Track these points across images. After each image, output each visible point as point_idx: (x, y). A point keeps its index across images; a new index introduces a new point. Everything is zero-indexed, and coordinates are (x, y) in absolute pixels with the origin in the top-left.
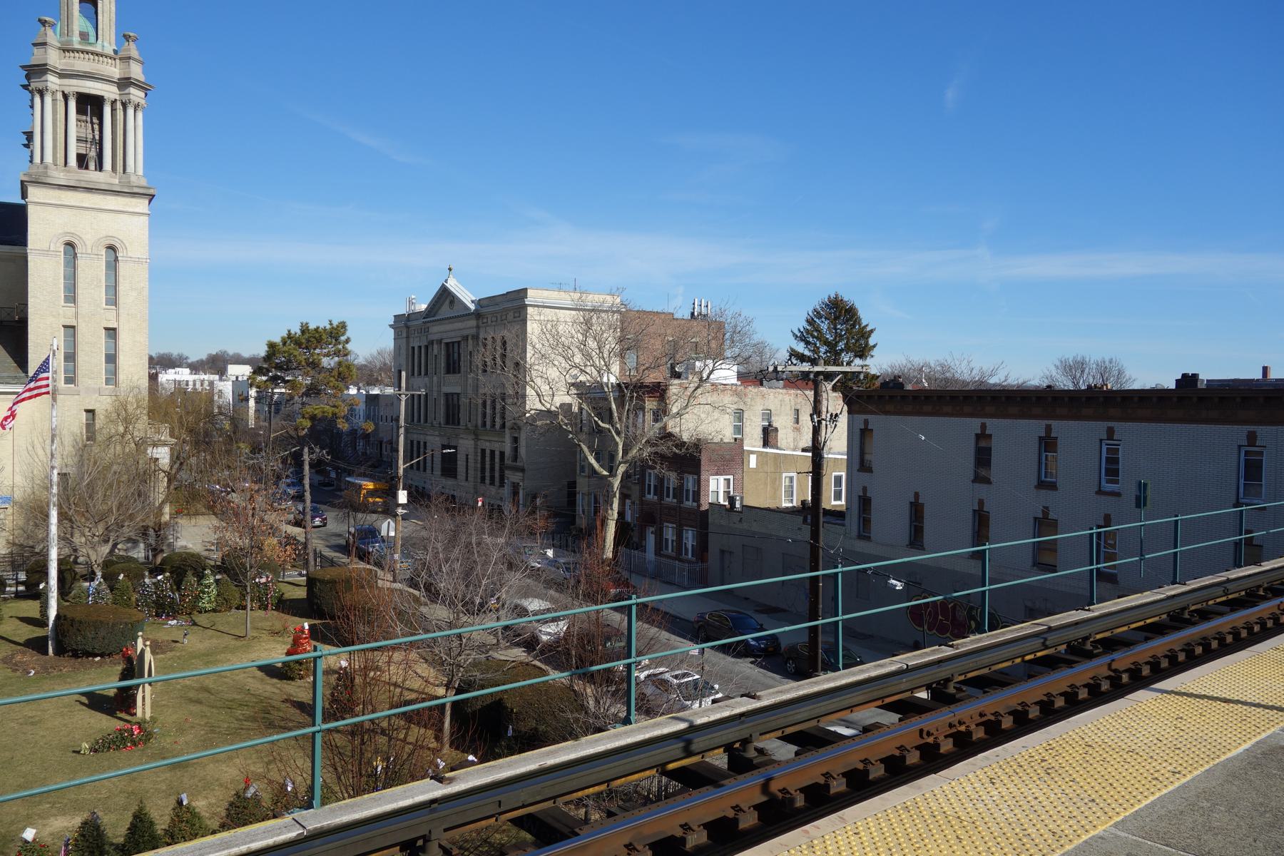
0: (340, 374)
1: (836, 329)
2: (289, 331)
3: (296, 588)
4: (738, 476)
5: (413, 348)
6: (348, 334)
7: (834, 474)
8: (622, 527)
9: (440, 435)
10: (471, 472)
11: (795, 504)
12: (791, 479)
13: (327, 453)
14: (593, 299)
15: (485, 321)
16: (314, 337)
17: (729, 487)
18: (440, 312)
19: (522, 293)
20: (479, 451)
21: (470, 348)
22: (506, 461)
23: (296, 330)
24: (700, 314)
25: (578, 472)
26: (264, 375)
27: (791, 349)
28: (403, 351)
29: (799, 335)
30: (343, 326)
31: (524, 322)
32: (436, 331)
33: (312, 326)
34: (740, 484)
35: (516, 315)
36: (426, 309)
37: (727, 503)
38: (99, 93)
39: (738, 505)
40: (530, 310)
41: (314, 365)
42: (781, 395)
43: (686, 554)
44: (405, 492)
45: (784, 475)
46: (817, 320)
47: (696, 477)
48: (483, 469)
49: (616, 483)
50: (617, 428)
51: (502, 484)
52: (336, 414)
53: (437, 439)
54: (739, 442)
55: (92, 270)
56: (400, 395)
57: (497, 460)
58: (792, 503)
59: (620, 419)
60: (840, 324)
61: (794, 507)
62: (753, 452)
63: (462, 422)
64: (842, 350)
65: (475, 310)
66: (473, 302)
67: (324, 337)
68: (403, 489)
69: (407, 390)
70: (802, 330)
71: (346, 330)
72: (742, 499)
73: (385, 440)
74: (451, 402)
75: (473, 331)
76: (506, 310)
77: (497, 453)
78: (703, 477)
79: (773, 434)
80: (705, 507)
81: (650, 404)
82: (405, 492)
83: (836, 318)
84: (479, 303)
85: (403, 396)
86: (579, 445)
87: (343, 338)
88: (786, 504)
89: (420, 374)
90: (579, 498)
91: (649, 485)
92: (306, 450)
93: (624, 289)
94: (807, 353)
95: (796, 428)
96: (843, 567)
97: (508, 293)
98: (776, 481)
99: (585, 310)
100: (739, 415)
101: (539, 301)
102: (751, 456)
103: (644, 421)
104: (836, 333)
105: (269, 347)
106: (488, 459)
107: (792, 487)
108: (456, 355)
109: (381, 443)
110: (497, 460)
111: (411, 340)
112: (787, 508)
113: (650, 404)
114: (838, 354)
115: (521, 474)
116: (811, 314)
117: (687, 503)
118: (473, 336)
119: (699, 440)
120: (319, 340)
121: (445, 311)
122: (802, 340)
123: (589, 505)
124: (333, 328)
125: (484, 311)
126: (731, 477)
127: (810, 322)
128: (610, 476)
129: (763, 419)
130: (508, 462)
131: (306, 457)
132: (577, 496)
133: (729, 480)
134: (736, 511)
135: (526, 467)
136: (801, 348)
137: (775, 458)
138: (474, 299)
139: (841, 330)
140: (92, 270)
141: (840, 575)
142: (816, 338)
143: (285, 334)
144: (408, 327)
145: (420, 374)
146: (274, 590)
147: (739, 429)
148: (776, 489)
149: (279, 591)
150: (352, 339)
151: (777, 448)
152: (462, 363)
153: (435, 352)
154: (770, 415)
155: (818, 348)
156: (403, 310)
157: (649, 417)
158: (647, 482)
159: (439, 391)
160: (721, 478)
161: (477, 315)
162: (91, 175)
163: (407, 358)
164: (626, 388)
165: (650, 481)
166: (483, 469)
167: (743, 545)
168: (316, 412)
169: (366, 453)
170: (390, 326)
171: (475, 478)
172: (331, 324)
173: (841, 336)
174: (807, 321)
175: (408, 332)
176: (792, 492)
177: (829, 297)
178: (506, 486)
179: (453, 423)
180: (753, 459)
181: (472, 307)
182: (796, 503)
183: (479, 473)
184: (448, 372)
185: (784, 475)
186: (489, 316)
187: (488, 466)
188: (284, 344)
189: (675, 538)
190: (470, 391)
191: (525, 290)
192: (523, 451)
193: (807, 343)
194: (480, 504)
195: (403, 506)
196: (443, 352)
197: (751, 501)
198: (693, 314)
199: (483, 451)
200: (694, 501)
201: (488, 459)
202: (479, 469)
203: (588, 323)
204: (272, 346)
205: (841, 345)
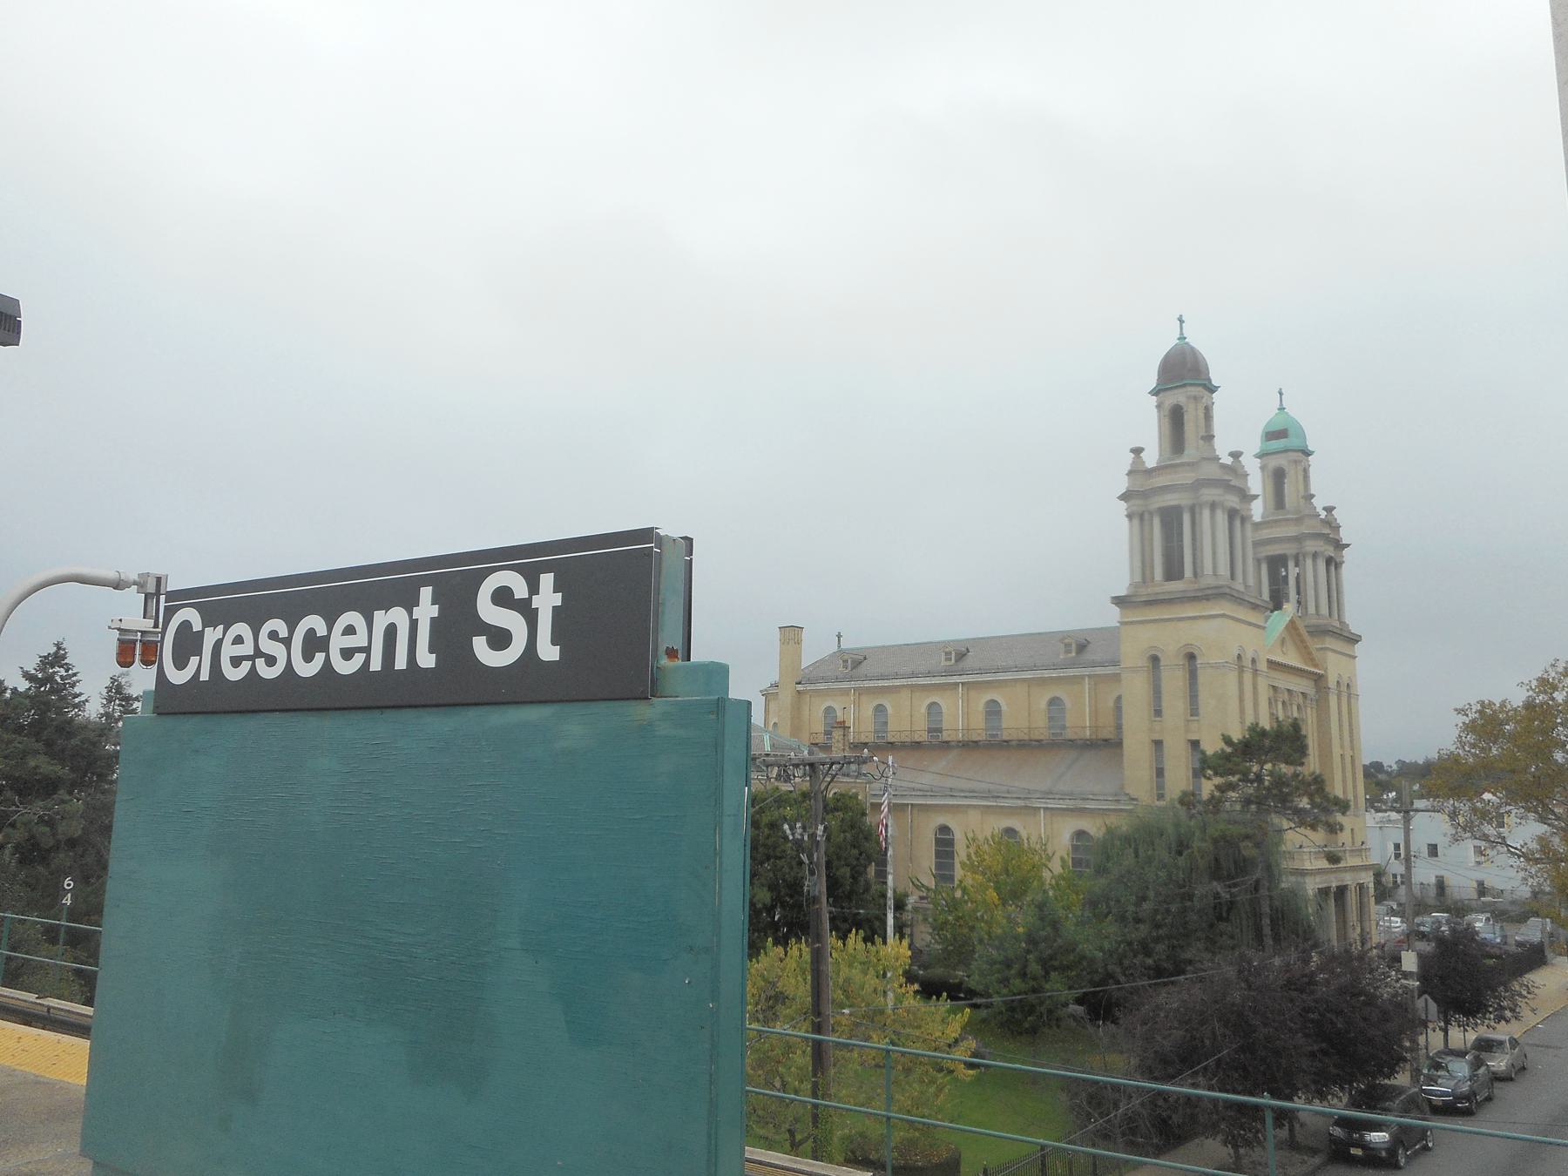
55: (1173, 681)
140: (1173, 681)
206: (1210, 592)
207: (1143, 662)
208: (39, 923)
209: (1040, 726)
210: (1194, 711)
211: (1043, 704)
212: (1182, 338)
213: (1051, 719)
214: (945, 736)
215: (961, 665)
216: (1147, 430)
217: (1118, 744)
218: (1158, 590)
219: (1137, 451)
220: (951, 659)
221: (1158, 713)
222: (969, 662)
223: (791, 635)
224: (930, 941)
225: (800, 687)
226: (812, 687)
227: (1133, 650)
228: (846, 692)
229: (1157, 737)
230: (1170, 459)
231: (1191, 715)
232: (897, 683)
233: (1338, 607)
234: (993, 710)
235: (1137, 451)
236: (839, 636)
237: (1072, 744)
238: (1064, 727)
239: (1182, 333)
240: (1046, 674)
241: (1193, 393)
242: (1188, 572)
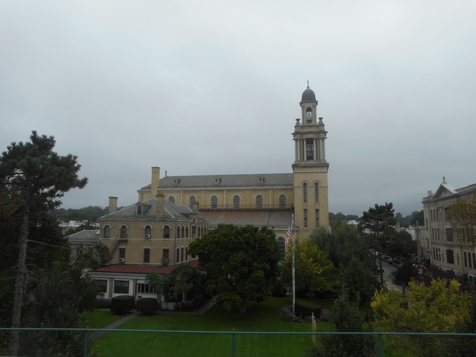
2: (370, 208)
5: (431, 210)
10: (460, 262)
33: (379, 205)
38: (312, 137)
55: (311, 192)
57: (472, 257)
87: (391, 210)
89: (435, 221)
110: (472, 257)
121: (444, 195)
140: (311, 192)
145: (435, 221)
153: (440, 211)
159: (443, 227)
162: (311, 162)
202: (464, 261)
204: (365, 213)
206: (323, 165)
207: (302, 185)
208: (19, 330)
209: (209, 205)
210: (317, 200)
211: (255, 197)
212: (308, 87)
213: (257, 202)
214: (218, 207)
215: (179, 185)
216: (298, 113)
217: (292, 210)
218: (306, 163)
219: (298, 120)
220: (218, 182)
221: (305, 201)
222: (181, 183)
223: (156, 170)
224: (324, 278)
225: (160, 189)
226: (165, 189)
227: (298, 181)
228: (179, 191)
229: (305, 208)
230: (307, 124)
231: (316, 202)
232: (200, 189)
233: (317, 172)
234: (214, 199)
235: (298, 120)
236: (166, 172)
237: (265, 210)
238: (262, 205)
239: (308, 86)
240: (257, 188)
241: (314, 105)
242: (315, 158)
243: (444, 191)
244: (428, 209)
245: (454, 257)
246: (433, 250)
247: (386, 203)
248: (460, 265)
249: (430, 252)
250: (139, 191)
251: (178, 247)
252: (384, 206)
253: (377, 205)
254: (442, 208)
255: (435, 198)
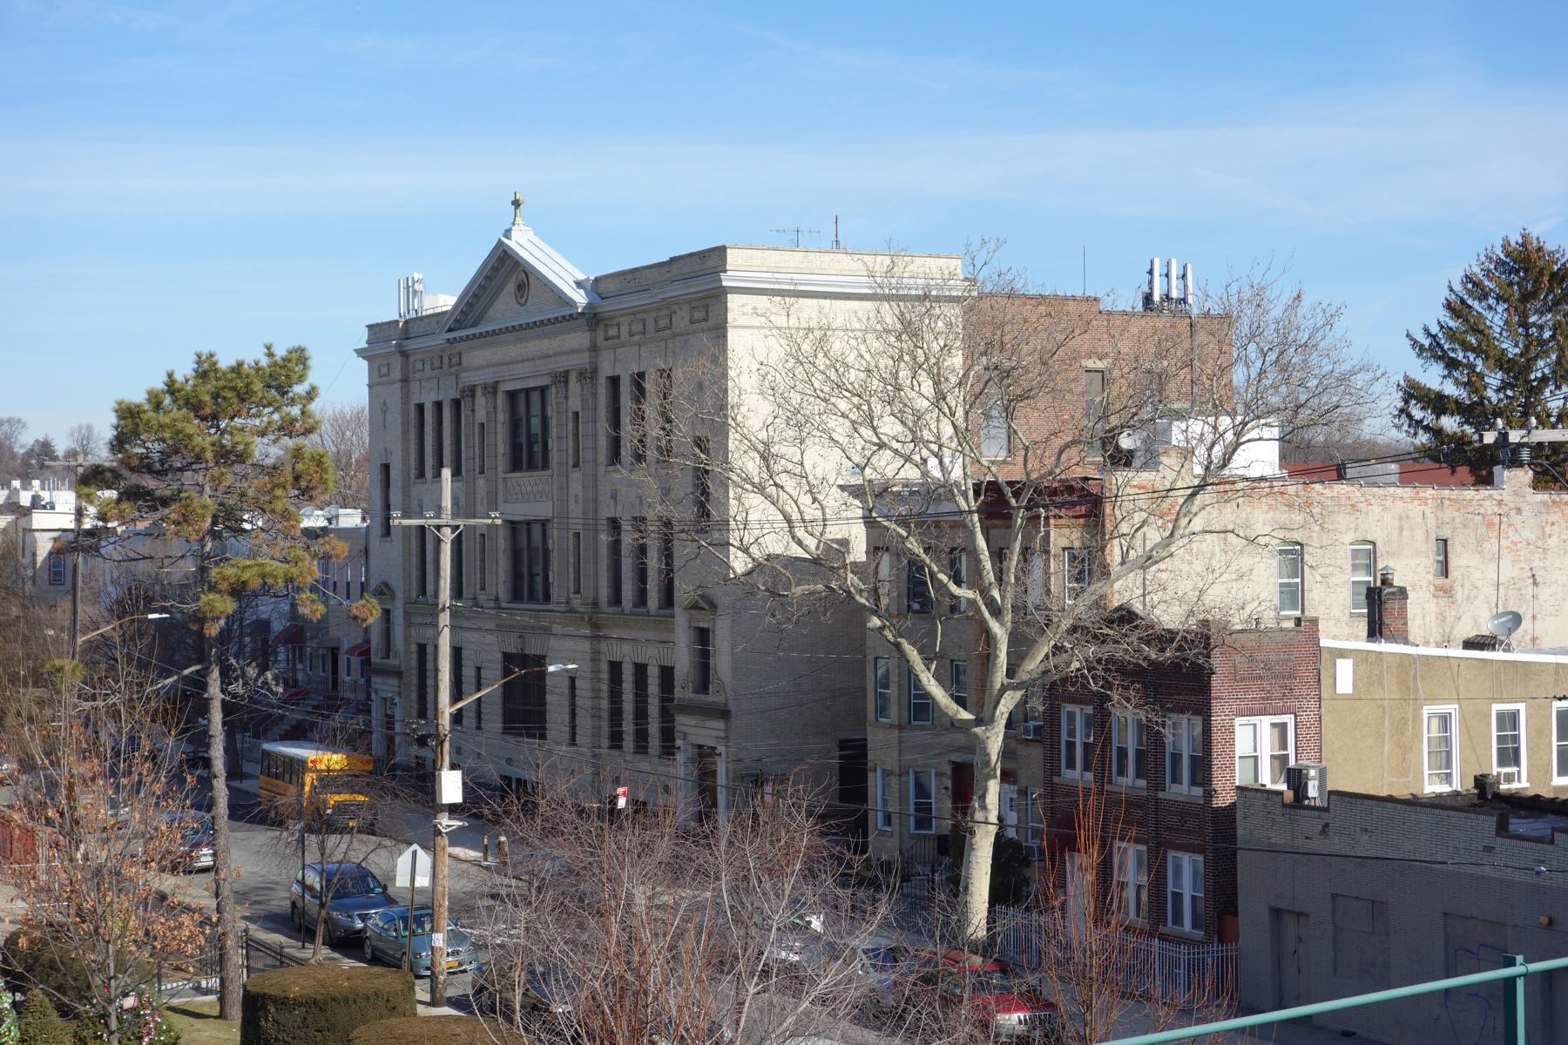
0: (297, 478)
1: (1526, 326)
2: (170, 375)
3: (199, 1023)
4: (1308, 716)
5: (421, 407)
6: (313, 378)
7: (1497, 707)
8: (1005, 851)
9: (500, 628)
10: (584, 721)
11: (1456, 785)
12: (1445, 720)
13: (276, 678)
14: (921, 270)
15: (612, 332)
16: (234, 389)
17: (1284, 746)
18: (491, 312)
19: (717, 256)
20: (605, 667)
21: (575, 404)
22: (678, 693)
23: (185, 370)
24: (1168, 297)
25: (871, 716)
26: (109, 488)
27: (1407, 379)
28: (395, 418)
29: (1426, 342)
30: (299, 357)
31: (719, 331)
32: (482, 363)
33: (225, 362)
34: (1313, 737)
35: (696, 315)
36: (455, 307)
37: (1283, 787)
39: (1313, 791)
40: (733, 301)
41: (229, 456)
42: (1399, 504)
43: (1178, 918)
44: (458, 774)
45: (1427, 710)
46: (1476, 304)
47: (1198, 722)
48: (616, 714)
49: (995, 740)
50: (993, 599)
51: (668, 750)
52: (291, 580)
53: (490, 638)
54: (1307, 627)
56: (438, 528)
57: (653, 688)
58: (1448, 778)
59: (1000, 579)
60: (1537, 311)
61: (1456, 794)
62: (1342, 653)
63: (555, 592)
64: (1544, 380)
65: (589, 306)
66: (579, 284)
67: (258, 386)
68: (453, 767)
69: (455, 515)
70: (1435, 329)
71: (306, 368)
72: (1323, 774)
73: (345, 646)
74: (523, 543)
75: (583, 360)
76: (670, 306)
77: (653, 673)
78: (1217, 720)
79: (1392, 606)
80: (1224, 799)
81: (1063, 535)
82: (458, 774)
83: (1526, 297)
84: (596, 287)
85: (448, 530)
86: (897, 646)
87: (299, 389)
88: (1432, 787)
90: (875, 782)
91: (1071, 746)
92: (215, 674)
93: (1000, 243)
94: (1450, 389)
95: (1441, 589)
96: (1528, 961)
97: (673, 260)
98: (1405, 726)
99: (904, 298)
100: (1294, 557)
101: (764, 280)
102: (1339, 662)
103: (1047, 574)
104: (1527, 335)
105: (121, 417)
106: (628, 687)
107: (1447, 741)
108: (536, 422)
109: (334, 653)
110: (653, 688)
111: (415, 386)
112: (1439, 796)
113: (1063, 535)
114: (1534, 391)
115: (720, 724)
116: (1458, 288)
117: (1175, 788)
118: (581, 374)
119: (1205, 623)
120: (244, 396)
121: (504, 311)
122: (1438, 358)
123: (903, 798)
124: (275, 364)
125: (607, 307)
126: (1289, 719)
127: (1456, 309)
128: (979, 721)
129: (1355, 567)
130: (683, 692)
131: (214, 689)
132: (870, 775)
133: (1282, 727)
134: (1309, 808)
135: (732, 706)
136: (1433, 377)
137: (1401, 665)
138: (581, 277)
139: (1541, 328)
141: (1520, 984)
142: (1473, 350)
143: (159, 384)
144: (405, 354)
146: (158, 1025)
147: (1293, 595)
148: (1407, 749)
149: (169, 1030)
150: (322, 391)
151: (1406, 642)
152: (553, 444)
153: (481, 415)
154: (1372, 555)
155: (1481, 376)
156: (389, 311)
157: (1059, 568)
158: (1064, 737)
160: (1265, 722)
161: (593, 318)
163: (405, 432)
164: (1017, 495)
165: (1072, 733)
166: (616, 714)
167: (1334, 896)
168: (246, 576)
169: (296, 681)
170: (360, 352)
171: (596, 735)
172: (270, 355)
173: (1542, 342)
174: (1449, 306)
175: (405, 368)
176: (1449, 754)
177: (1506, 245)
178: (680, 757)
179: (532, 598)
180: (1345, 669)
181: (580, 298)
182: (1459, 782)
183: (605, 724)
184: (516, 465)
185: (1427, 710)
186: (625, 321)
187: (628, 705)
188: (158, 406)
189: (1144, 880)
190: (576, 510)
191: (719, 253)
192: (722, 664)
193: (1452, 364)
194: (622, 802)
195: (453, 809)
196: (502, 417)
197: (1343, 781)
198: (1148, 299)
199: (615, 668)
200: (1193, 783)
201: (628, 687)
202: (605, 714)
203: (908, 328)
205: (1542, 367)
243: (511, 287)
244: (398, 393)
245: (549, 698)
246: (415, 656)
247: (269, 348)
248: (579, 740)
249: (398, 674)
250: (370, 327)
251: (415, 400)
252: (258, 369)
253: (215, 364)
254: (495, 393)
255: (450, 330)
